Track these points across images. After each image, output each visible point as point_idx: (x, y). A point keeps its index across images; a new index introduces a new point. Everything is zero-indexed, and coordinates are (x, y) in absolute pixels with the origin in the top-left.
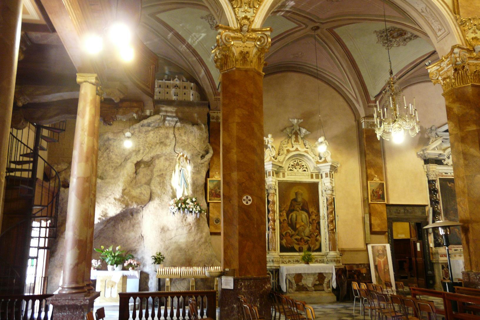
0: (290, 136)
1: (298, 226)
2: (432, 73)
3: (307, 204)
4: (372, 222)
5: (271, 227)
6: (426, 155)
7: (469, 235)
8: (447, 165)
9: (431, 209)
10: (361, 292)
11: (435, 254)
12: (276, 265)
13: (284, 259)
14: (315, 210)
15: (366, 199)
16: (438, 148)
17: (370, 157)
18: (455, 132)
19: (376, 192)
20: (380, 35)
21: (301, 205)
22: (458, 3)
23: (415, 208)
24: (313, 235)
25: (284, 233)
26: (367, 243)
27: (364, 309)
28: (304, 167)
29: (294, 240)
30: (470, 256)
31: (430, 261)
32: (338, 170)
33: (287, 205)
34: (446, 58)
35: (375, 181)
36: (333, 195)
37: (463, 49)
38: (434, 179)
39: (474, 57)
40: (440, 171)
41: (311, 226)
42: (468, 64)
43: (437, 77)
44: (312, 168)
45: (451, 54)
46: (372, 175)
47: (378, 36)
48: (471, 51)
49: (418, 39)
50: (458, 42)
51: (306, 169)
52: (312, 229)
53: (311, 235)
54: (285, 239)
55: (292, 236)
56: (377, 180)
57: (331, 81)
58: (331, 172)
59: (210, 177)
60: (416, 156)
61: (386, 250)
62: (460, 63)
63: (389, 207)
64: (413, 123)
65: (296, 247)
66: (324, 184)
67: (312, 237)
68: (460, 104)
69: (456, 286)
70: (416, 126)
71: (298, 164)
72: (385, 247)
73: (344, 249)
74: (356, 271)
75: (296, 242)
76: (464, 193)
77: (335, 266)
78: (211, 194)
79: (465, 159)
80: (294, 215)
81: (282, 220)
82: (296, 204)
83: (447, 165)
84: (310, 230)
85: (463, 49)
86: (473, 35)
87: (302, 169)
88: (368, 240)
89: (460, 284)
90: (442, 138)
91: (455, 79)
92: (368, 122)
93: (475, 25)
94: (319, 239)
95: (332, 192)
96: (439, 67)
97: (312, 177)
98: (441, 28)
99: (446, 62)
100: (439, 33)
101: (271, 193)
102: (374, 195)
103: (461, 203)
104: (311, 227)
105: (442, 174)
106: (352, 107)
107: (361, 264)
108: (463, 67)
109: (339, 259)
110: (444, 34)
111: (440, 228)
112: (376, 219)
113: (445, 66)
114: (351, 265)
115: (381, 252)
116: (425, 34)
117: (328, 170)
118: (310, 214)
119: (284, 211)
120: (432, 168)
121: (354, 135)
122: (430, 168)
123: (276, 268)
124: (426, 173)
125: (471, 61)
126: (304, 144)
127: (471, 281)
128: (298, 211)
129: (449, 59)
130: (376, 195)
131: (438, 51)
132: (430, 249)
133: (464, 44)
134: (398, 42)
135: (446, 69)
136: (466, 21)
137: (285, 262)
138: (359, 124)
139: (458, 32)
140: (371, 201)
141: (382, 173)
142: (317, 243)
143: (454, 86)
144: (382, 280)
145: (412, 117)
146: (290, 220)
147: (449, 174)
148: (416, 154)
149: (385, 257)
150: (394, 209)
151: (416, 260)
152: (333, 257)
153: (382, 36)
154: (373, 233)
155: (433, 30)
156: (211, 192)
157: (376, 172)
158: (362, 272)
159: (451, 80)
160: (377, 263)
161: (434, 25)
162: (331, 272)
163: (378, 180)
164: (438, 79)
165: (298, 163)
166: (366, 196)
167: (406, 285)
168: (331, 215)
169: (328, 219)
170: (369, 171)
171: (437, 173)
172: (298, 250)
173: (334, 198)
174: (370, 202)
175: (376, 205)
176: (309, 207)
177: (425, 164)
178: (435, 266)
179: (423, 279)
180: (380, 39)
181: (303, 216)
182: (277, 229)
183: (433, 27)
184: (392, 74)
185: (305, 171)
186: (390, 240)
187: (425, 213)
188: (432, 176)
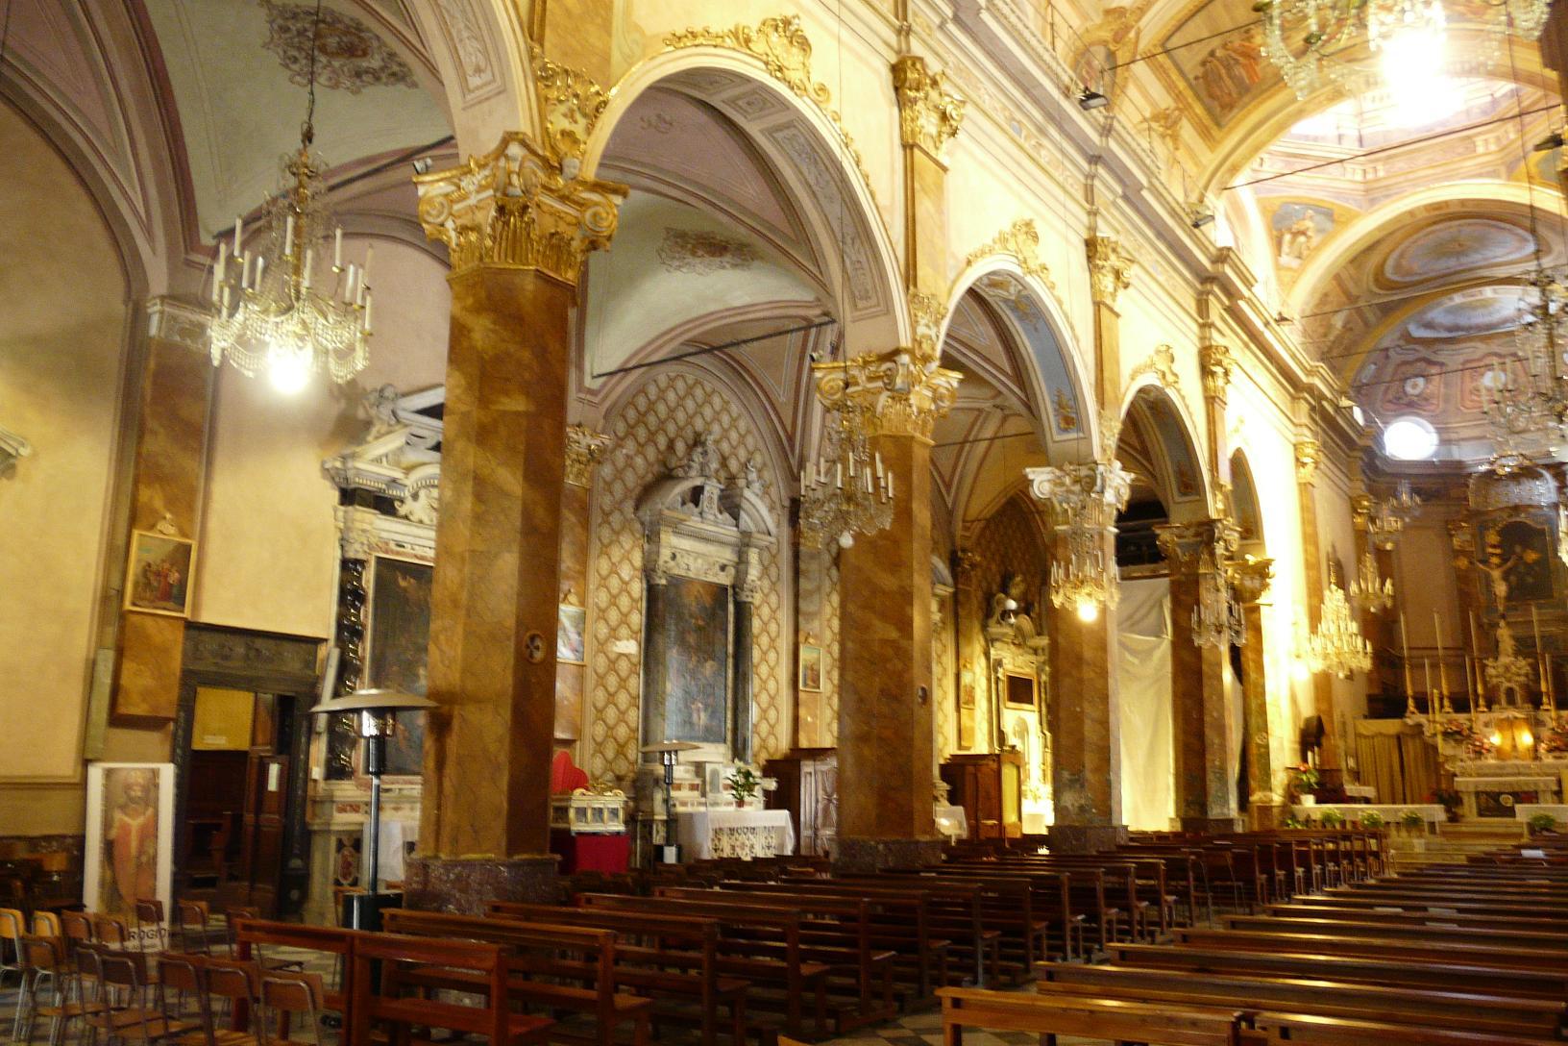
2: (430, 201)
4: (125, 681)
6: (350, 474)
7: (448, 740)
8: (406, 517)
9: (335, 653)
10: (34, 951)
11: (322, 802)
15: (113, 593)
16: (394, 458)
17: (157, 444)
18: (464, 408)
19: (158, 574)
20: (280, 21)
22: (544, 9)
23: (287, 645)
26: (90, 756)
27: (34, 1010)
30: (439, 808)
31: (304, 825)
32: (21, 468)
34: (482, 167)
35: (161, 532)
37: (534, 152)
38: (361, 556)
39: (559, 190)
40: (385, 535)
42: (538, 206)
43: (442, 218)
45: (497, 159)
47: (271, 22)
48: (552, 167)
49: (401, 87)
50: (523, 126)
56: (168, 531)
57: (56, 125)
60: (319, 474)
61: (157, 786)
62: (518, 192)
63: (194, 633)
64: (349, 333)
68: (494, 323)
69: (390, 906)
70: (358, 346)
72: (155, 773)
74: (25, 862)
76: (455, 604)
79: (479, 497)
83: (406, 517)
85: (534, 152)
86: (566, 124)
88: (96, 745)
89: (395, 901)
90: (407, 430)
91: (494, 238)
93: (576, 96)
96: (453, 188)
98: (482, 64)
99: (480, 177)
100: (474, 81)
102: (148, 584)
103: (442, 637)
105: (387, 544)
106: (125, 249)
107: (48, 838)
108: (525, 208)
110: (490, 88)
111: (365, 715)
113: (472, 188)
115: (139, 794)
116: (433, 70)
120: (362, 521)
121: (111, 350)
122: (353, 520)
124: (339, 535)
125: (548, 200)
127: (430, 888)
129: (487, 172)
130: (155, 584)
131: (460, 139)
132: (311, 785)
133: (539, 139)
134: (334, 72)
135: (472, 201)
136: (555, 74)
138: (138, 316)
139: (529, 99)
140: (134, 604)
141: (191, 508)
143: (487, 260)
145: (348, 310)
147: (408, 549)
149: (150, 811)
150: (211, 642)
151: (257, 820)
153: (287, 30)
155: (459, 65)
157: (171, 503)
158: (47, 867)
159: (481, 239)
160: (113, 834)
161: (464, 48)
163: (172, 530)
164: (442, 225)
166: (115, 583)
167: (213, 910)
170: (145, 494)
171: (373, 540)
174: (128, 606)
175: (149, 622)
177: (342, 503)
178: (318, 843)
179: (269, 887)
180: (276, 36)
183: (461, 53)
184: (310, 141)
186: (178, 751)
188: (357, 546)
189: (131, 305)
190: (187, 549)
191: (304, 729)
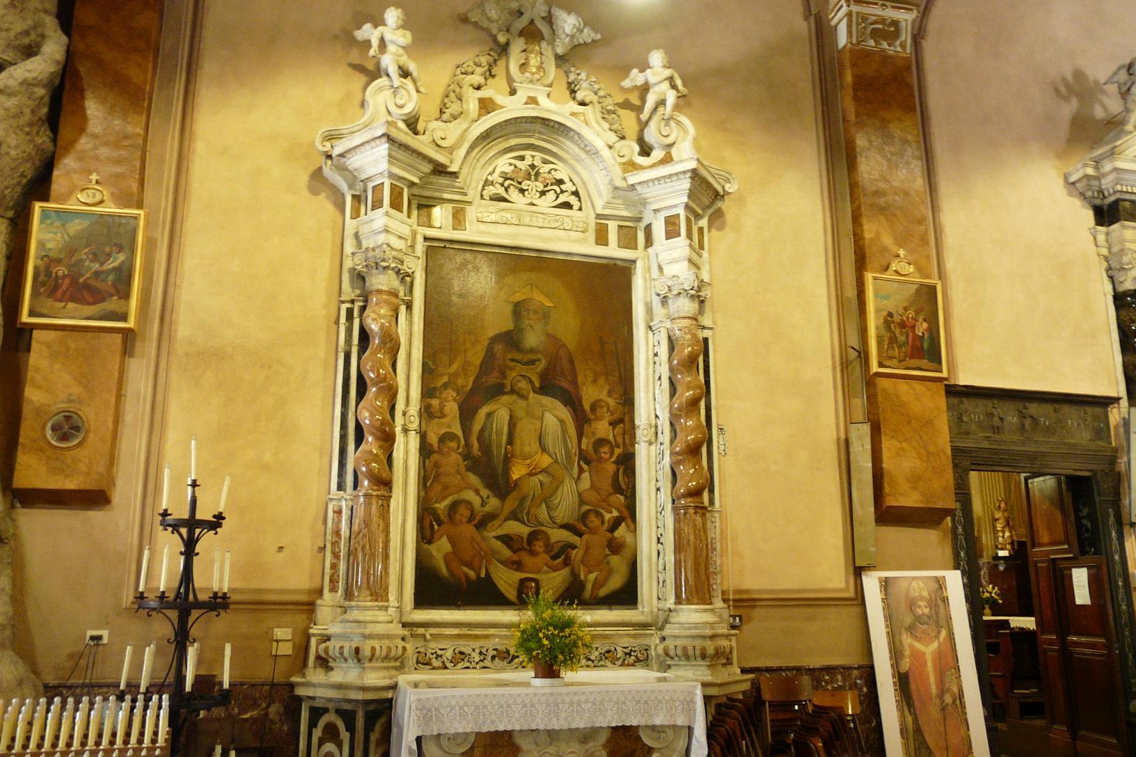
0: (502, 39)
1: (517, 473)
3: (571, 361)
4: (886, 465)
5: (364, 469)
6: (1107, 183)
12: (375, 678)
13: (434, 645)
14: (610, 394)
19: (902, 325)
21: (541, 365)
23: (1067, 409)
24: (594, 521)
25: (442, 506)
26: (858, 564)
28: (563, 187)
29: (498, 545)
33: (466, 364)
36: (704, 328)
41: (586, 475)
44: (601, 195)
46: (885, 249)
51: (573, 200)
52: (592, 486)
53: (584, 517)
54: (445, 538)
55: (482, 523)
58: (698, 217)
59: (52, 197)
60: (1065, 191)
61: (945, 600)
65: (506, 580)
66: (660, 268)
67: (593, 531)
71: (533, 173)
72: (940, 584)
73: (748, 591)
75: (507, 553)
77: (705, 685)
78: (43, 284)
80: (502, 416)
81: (433, 439)
82: (513, 360)
84: (580, 495)
87: (551, 196)
88: (867, 550)
92: (864, 19)
94: (629, 538)
95: (696, 305)
97: (602, 238)
101: (379, 292)
102: (893, 340)
104: (586, 482)
107: (829, 670)
109: (724, 643)
112: (903, 449)
114: (789, 677)
115: (926, 611)
117: (675, 197)
118: (583, 411)
119: (451, 393)
123: (370, 696)
124: (1105, 265)
126: (569, 84)
128: (524, 397)
130: (902, 339)
137: (436, 663)
141: (924, 240)
142: (618, 563)
144: (932, 747)
146: (478, 439)
148: (1061, 181)
149: (944, 633)
150: (975, 410)
152: (694, 632)
154: (887, 516)
156: (48, 273)
160: (905, 665)
162: (681, 721)
165: (533, 166)
166: (854, 341)
168: (688, 416)
169: (672, 442)
170: (870, 229)
172: (511, 594)
173: (706, 340)
174: (875, 368)
175: (902, 386)
176: (580, 379)
181: (550, 421)
182: (406, 484)
185: (567, 205)
187: (1109, 436)
189: (812, 18)
190: (933, 289)
191: (1112, 519)
